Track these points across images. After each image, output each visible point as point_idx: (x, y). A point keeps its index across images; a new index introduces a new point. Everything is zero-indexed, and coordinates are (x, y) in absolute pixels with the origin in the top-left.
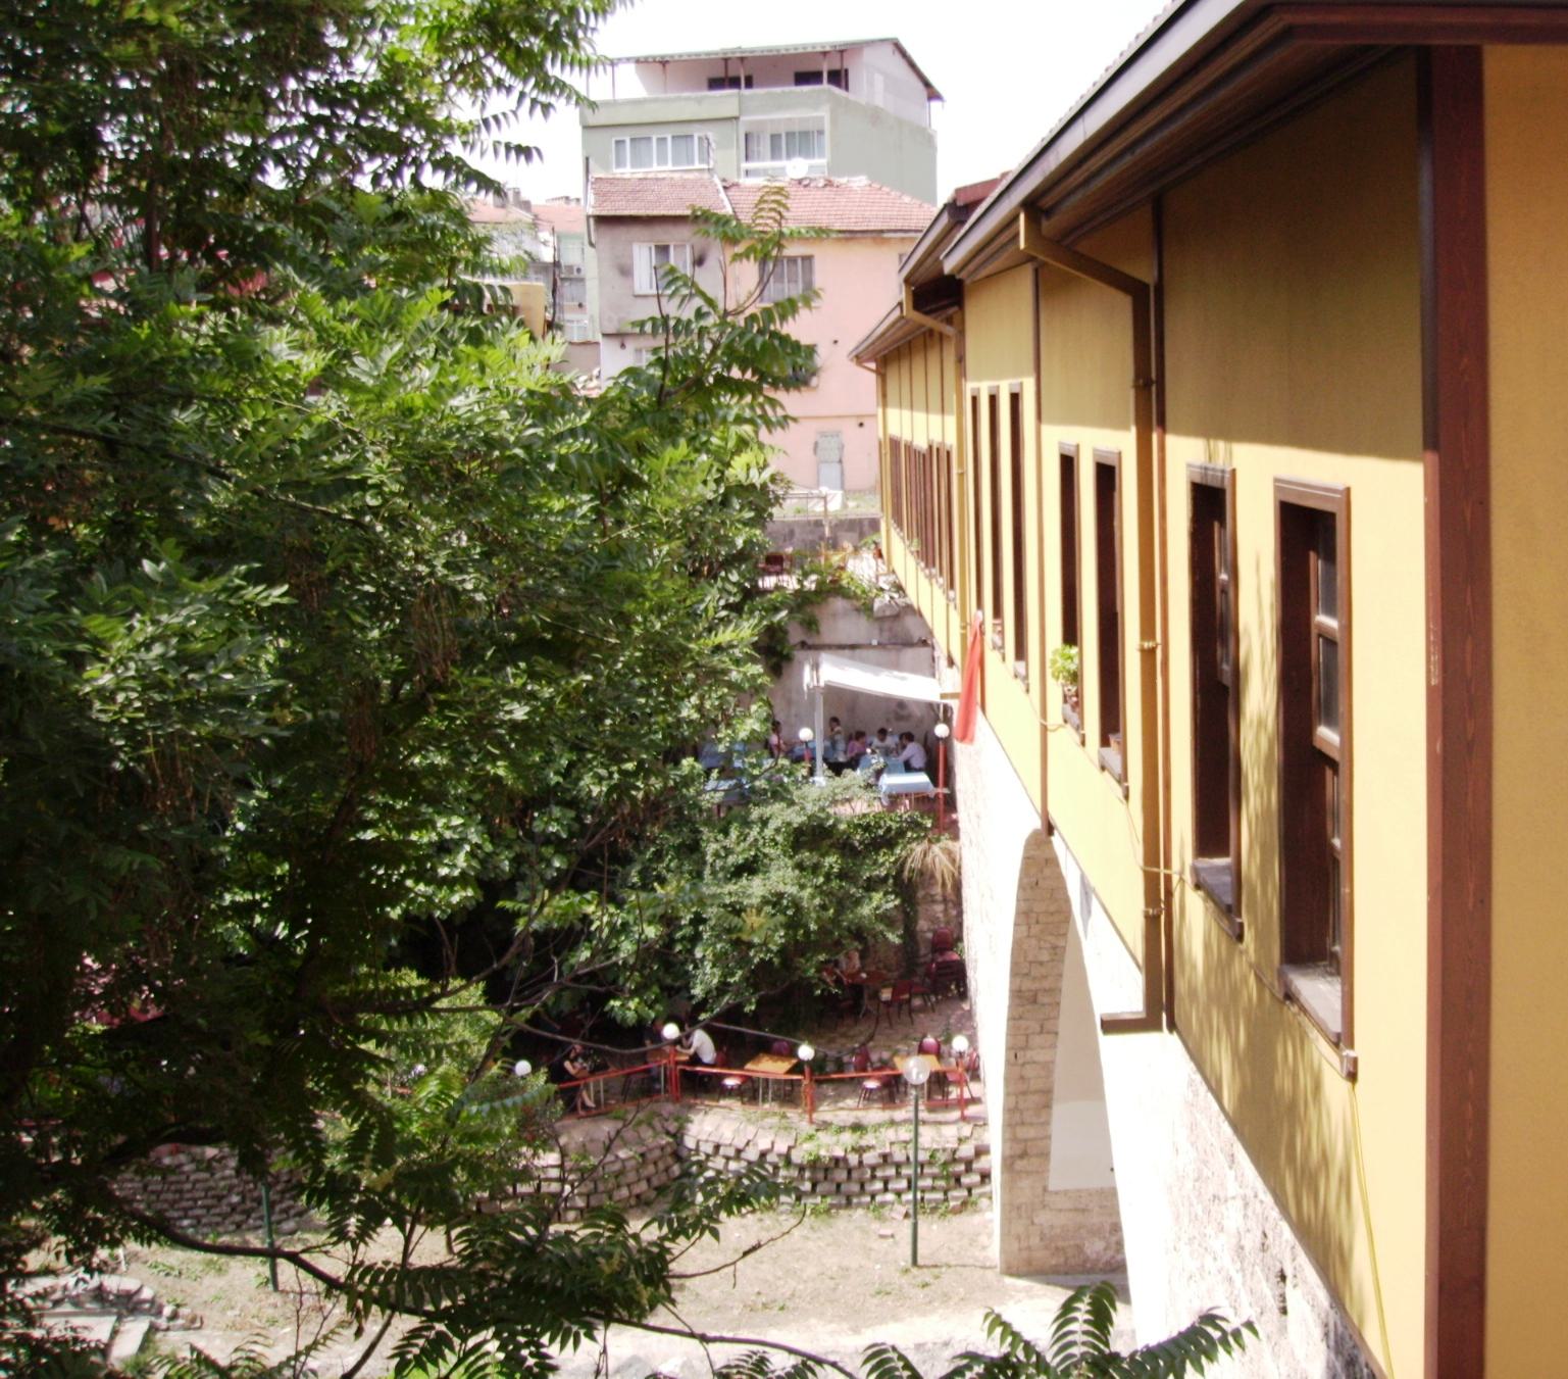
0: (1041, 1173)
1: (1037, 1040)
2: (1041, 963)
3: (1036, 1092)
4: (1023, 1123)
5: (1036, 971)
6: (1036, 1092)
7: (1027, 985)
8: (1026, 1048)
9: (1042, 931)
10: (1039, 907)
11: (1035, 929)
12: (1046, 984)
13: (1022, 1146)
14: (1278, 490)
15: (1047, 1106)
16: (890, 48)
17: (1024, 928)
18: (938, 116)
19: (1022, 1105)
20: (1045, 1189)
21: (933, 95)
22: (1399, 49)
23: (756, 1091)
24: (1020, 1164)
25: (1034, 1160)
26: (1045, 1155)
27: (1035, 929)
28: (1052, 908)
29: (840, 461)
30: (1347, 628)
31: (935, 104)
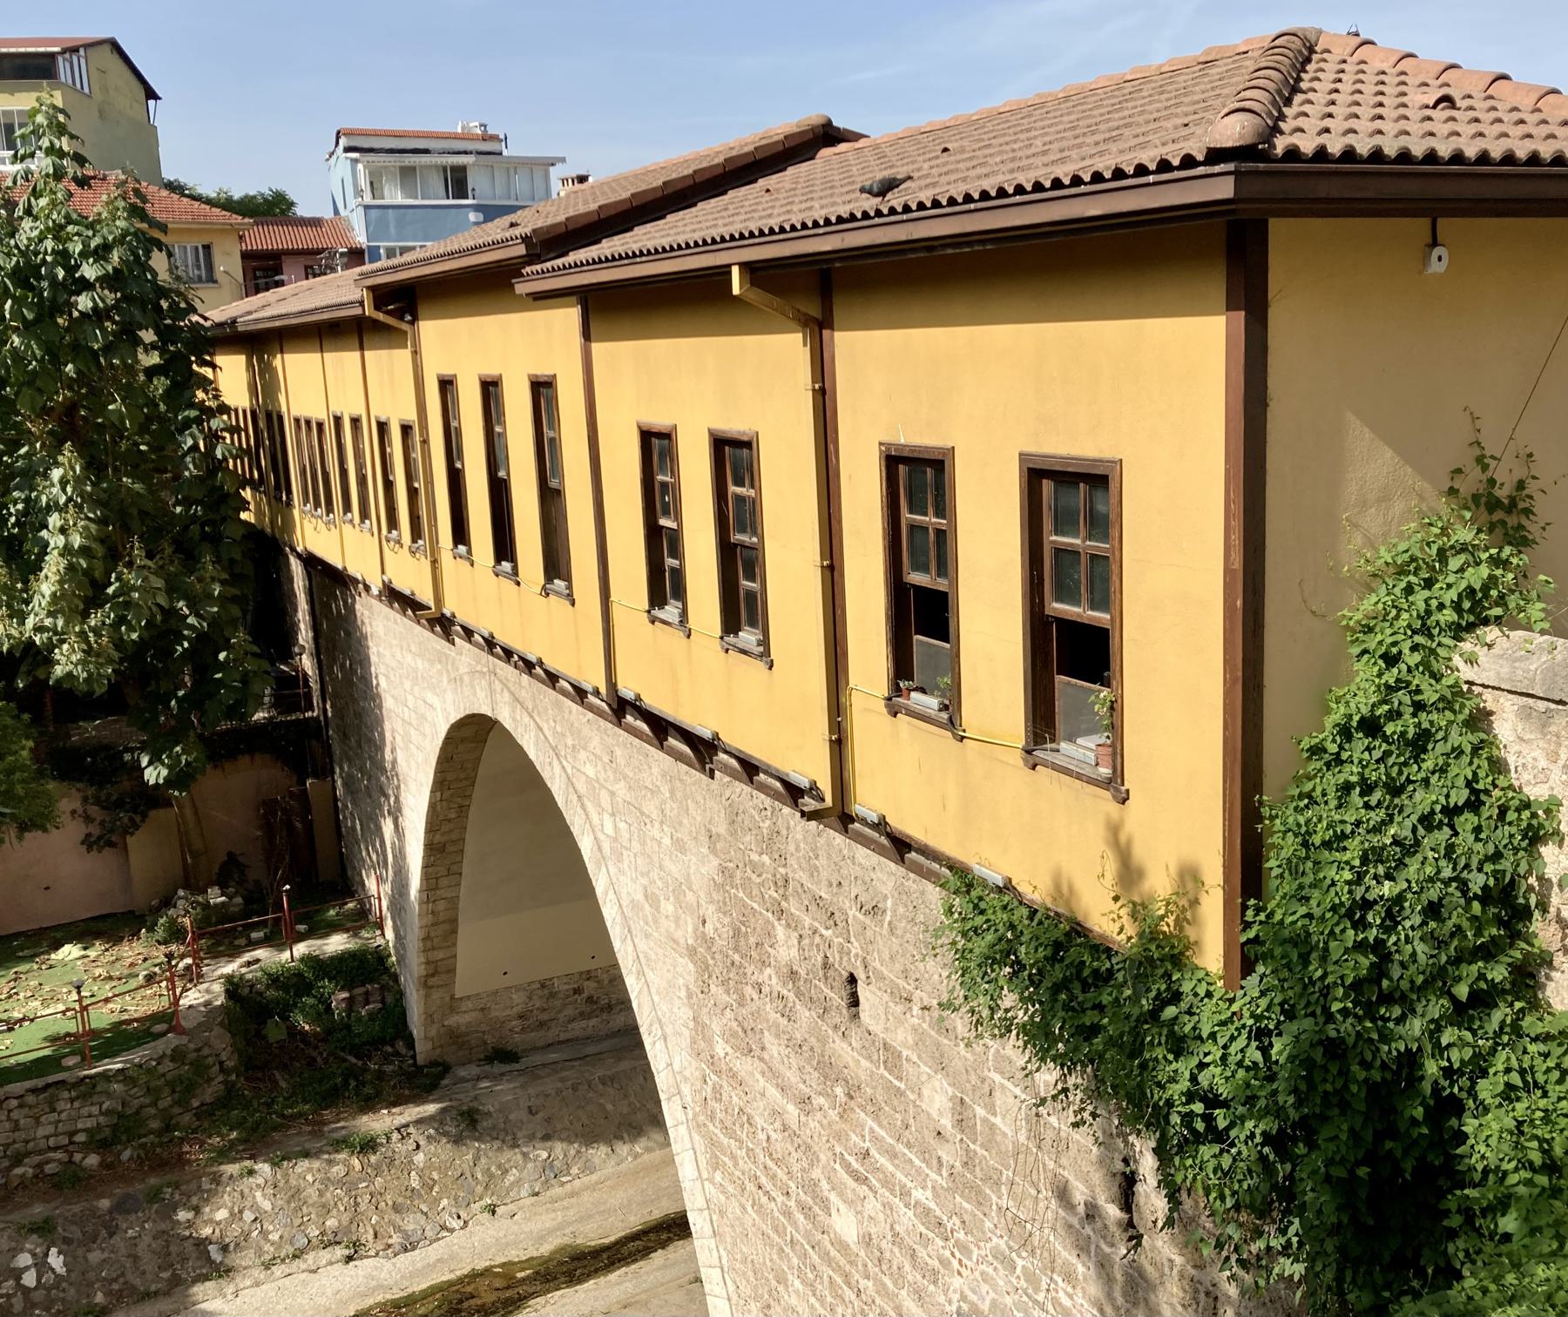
0: (449, 985)
1: (444, 882)
2: (449, 821)
3: (444, 922)
4: (433, 949)
5: (445, 828)
6: (444, 922)
7: (438, 838)
8: (437, 888)
9: (452, 795)
10: (450, 776)
11: (447, 794)
12: (454, 836)
13: (433, 966)
14: (639, 427)
15: (454, 932)
16: (107, 48)
17: (438, 794)
18: (160, 114)
19: (433, 934)
20: (452, 997)
21: (151, 94)
22: (1291, 134)
23: (1489, 952)
24: (431, 981)
25: (444, 976)
26: (452, 971)
27: (447, 794)
28: (462, 776)
29: (1511, 438)
30: (680, 525)
31: (151, 103)
